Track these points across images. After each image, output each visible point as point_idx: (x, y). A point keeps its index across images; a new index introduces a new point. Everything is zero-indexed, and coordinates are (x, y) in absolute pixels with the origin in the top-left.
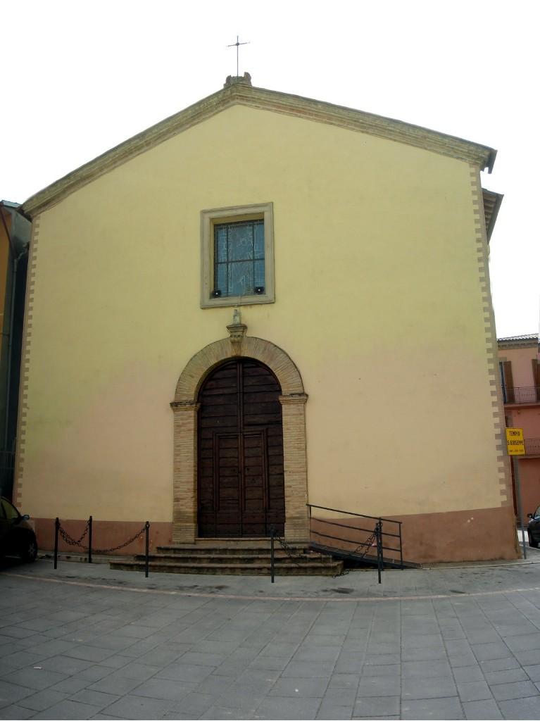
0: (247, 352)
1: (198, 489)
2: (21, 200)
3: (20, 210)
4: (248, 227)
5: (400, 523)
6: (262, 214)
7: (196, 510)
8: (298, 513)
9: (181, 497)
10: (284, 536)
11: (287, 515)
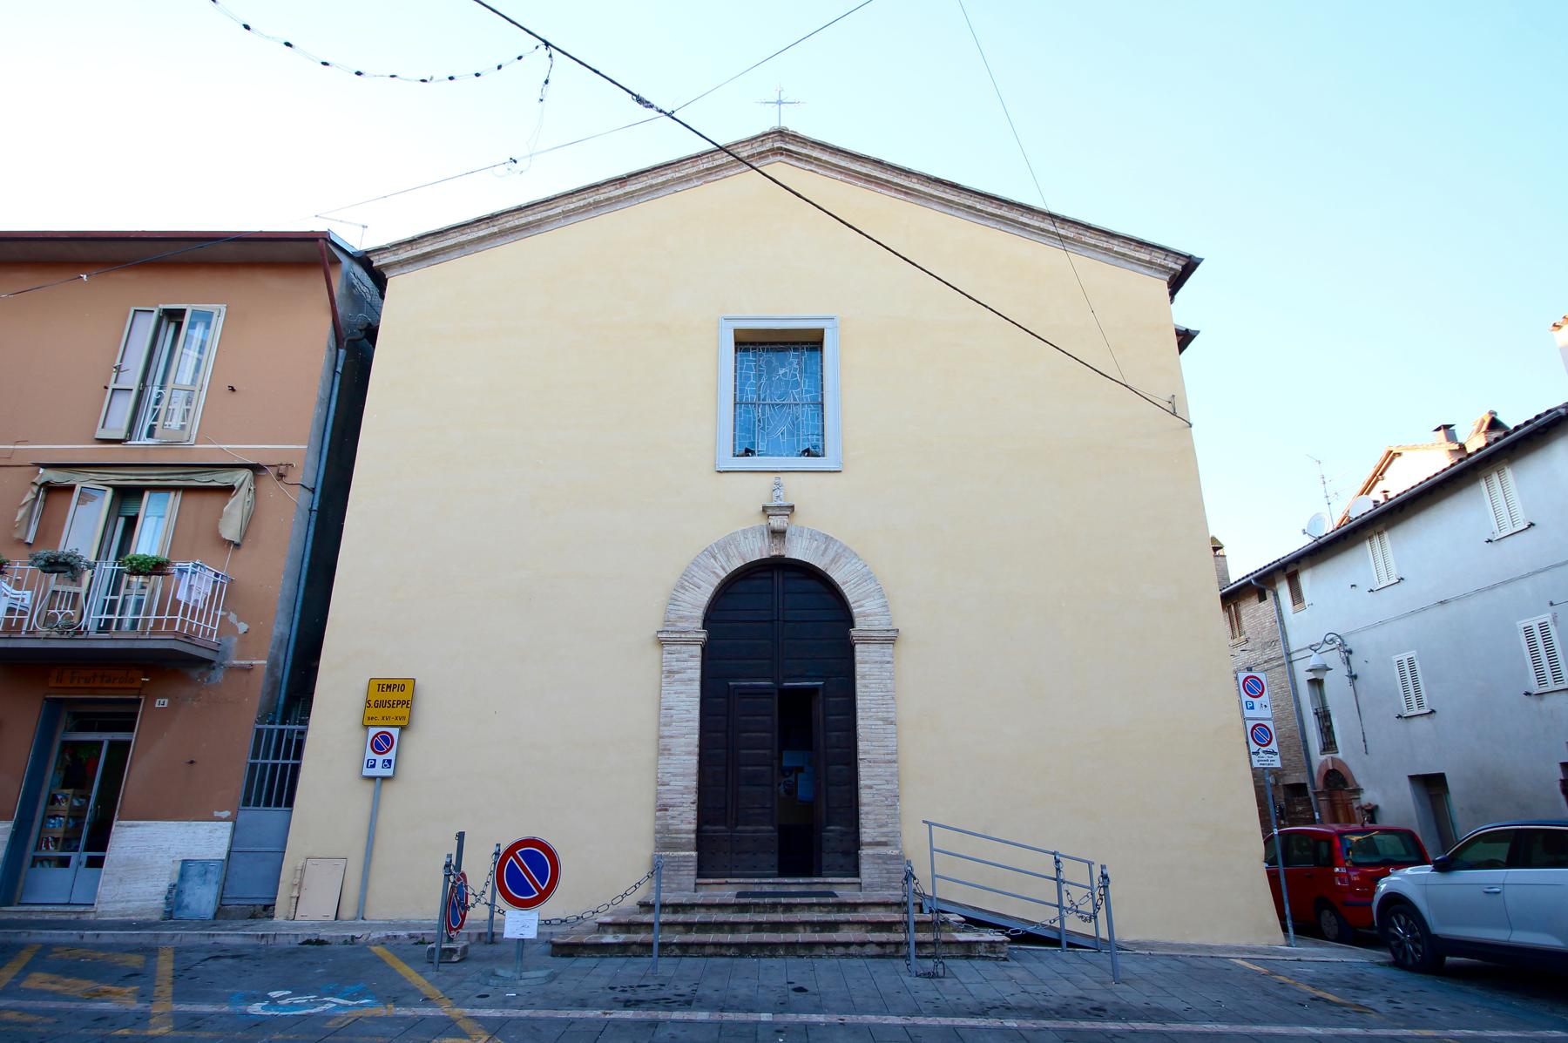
0: (797, 550)
3: (364, 260)
4: (792, 353)
6: (822, 331)
8: (884, 834)
9: (671, 802)
10: (858, 875)
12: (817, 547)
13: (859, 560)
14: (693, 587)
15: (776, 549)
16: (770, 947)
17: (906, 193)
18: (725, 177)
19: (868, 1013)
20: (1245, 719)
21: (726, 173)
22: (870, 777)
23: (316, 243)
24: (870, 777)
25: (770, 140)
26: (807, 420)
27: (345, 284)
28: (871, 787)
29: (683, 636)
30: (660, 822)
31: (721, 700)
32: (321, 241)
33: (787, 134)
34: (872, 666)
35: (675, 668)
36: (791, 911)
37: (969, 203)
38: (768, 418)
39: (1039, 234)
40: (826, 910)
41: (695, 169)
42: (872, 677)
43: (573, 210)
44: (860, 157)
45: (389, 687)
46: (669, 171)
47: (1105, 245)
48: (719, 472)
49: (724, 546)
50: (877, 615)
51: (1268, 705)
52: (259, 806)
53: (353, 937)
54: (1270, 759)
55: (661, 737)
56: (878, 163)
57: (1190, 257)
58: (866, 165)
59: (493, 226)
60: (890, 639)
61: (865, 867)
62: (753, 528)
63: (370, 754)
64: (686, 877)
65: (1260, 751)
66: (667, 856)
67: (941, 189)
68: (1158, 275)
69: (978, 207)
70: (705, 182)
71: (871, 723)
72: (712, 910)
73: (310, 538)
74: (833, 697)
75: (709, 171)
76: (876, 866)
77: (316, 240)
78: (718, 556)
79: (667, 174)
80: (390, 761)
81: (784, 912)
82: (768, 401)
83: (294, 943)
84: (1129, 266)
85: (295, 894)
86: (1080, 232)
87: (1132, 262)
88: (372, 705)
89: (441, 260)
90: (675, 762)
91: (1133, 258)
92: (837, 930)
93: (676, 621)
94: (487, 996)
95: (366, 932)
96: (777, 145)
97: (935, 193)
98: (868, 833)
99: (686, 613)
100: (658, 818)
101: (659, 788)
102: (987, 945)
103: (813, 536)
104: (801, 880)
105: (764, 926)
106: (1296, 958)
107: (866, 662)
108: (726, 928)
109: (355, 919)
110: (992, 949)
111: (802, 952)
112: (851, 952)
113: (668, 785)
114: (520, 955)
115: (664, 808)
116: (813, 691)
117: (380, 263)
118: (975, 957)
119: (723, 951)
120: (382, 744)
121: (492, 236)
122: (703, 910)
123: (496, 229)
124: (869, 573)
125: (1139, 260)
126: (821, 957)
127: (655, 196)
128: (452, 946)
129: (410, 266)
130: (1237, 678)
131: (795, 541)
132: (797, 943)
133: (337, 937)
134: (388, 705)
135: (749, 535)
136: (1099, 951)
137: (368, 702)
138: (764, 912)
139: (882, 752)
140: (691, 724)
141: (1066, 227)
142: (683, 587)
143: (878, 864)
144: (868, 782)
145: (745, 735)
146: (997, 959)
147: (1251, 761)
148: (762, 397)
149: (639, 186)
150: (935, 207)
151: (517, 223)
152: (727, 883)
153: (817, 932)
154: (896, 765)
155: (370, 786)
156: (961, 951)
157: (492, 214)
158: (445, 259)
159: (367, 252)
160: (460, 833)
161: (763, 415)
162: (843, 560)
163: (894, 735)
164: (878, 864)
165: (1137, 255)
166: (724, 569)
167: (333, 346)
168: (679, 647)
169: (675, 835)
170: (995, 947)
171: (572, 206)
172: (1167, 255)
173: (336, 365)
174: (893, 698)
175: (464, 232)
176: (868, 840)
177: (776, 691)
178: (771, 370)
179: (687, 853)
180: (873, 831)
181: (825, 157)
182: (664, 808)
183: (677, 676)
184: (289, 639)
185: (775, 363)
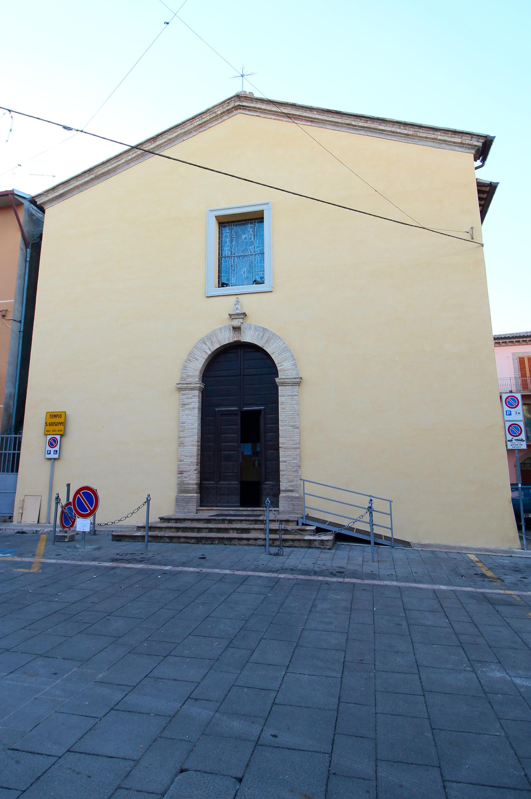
0: (248, 337)
1: (201, 463)
2: (33, 192)
3: (33, 201)
4: (249, 225)
5: (391, 502)
6: (262, 212)
7: (199, 482)
8: (292, 486)
9: (185, 470)
10: (278, 507)
11: (282, 488)
12: (259, 335)
13: (281, 340)
14: (195, 360)
15: (236, 337)
16: (211, 540)
17: (312, 121)
18: (210, 127)
19: (225, 569)
20: (505, 421)
21: (210, 125)
22: (285, 456)
23: (7, 197)
24: (285, 456)
25: (233, 102)
26: (257, 263)
27: (27, 215)
28: (285, 462)
29: (189, 386)
30: (179, 480)
31: (211, 418)
32: (10, 195)
33: (242, 97)
34: (287, 397)
35: (186, 402)
36: (232, 523)
37: (348, 122)
38: (236, 264)
39: (392, 135)
40: (249, 523)
41: (192, 126)
42: (287, 404)
43: (131, 159)
44: (283, 104)
45: (55, 416)
46: (179, 129)
47: (432, 136)
48: (207, 297)
49: (209, 338)
50: (290, 370)
51: (521, 413)
52: (5, 472)
53: (37, 531)
54: (519, 444)
55: (180, 438)
56: (293, 106)
57: (486, 137)
58: (287, 108)
59: (92, 174)
60: (298, 383)
61: (282, 503)
62: (225, 327)
63: (48, 448)
64: (192, 506)
65: (513, 439)
66: (182, 496)
67: (331, 116)
68: (468, 151)
69: (354, 123)
70: (199, 132)
71: (286, 428)
72: (194, 522)
73: (21, 345)
74: (269, 415)
75: (200, 125)
76: (287, 502)
77: (7, 195)
78: (207, 342)
79: (177, 131)
80: (57, 451)
81: (228, 523)
82: (237, 254)
83: (13, 532)
84: (449, 147)
85: (21, 512)
86: (416, 130)
87: (450, 145)
88: (48, 425)
89: (69, 196)
90: (186, 450)
91: (451, 142)
92: (249, 533)
93: (186, 378)
94: (60, 555)
95: (43, 529)
96: (237, 104)
97: (327, 119)
98: (283, 485)
99: (191, 374)
100: (179, 478)
101: (179, 463)
102: (320, 542)
103: (256, 328)
104: (248, 509)
105: (213, 529)
106: (509, 555)
107: (284, 396)
108: (195, 530)
109: (46, 523)
110: (322, 544)
111: (226, 542)
112: (250, 543)
113: (183, 461)
114: (84, 539)
115: (181, 473)
116: (259, 411)
117: (40, 202)
118: (313, 547)
119: (189, 541)
120: (52, 443)
121: (92, 180)
122: (189, 522)
123: (93, 176)
124: (286, 347)
125: (454, 143)
126: (235, 545)
127: (173, 145)
128: (65, 535)
129: (55, 202)
130: (501, 397)
131: (247, 332)
132: (223, 538)
133: (30, 530)
134: (54, 425)
135: (223, 330)
136: (393, 548)
137: (46, 423)
138: (219, 523)
139: (291, 443)
140: (194, 430)
141: (407, 128)
142: (189, 360)
143: (288, 501)
144: (284, 459)
145: (224, 435)
146: (324, 549)
147: (506, 446)
148: (233, 252)
149: (163, 141)
150: (329, 127)
151: (103, 171)
152: (212, 510)
153: (239, 533)
154: (299, 450)
155: (49, 463)
156: (306, 544)
157: (90, 168)
158: (71, 196)
159: (33, 197)
160: (68, 484)
161: (234, 262)
162: (272, 341)
163: (298, 434)
164: (288, 501)
165: (453, 140)
166: (210, 349)
167: (24, 248)
168: (187, 392)
169: (186, 486)
170: (324, 543)
171: (130, 157)
172: (472, 137)
173: (26, 257)
174: (298, 415)
175: (78, 180)
176: (284, 489)
177: (239, 413)
178: (238, 237)
179: (192, 495)
180: (286, 484)
181: (264, 106)
182: (181, 473)
183: (187, 406)
184: (15, 395)
185: (240, 233)
